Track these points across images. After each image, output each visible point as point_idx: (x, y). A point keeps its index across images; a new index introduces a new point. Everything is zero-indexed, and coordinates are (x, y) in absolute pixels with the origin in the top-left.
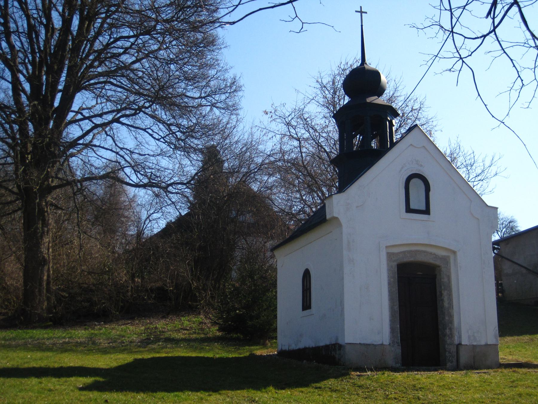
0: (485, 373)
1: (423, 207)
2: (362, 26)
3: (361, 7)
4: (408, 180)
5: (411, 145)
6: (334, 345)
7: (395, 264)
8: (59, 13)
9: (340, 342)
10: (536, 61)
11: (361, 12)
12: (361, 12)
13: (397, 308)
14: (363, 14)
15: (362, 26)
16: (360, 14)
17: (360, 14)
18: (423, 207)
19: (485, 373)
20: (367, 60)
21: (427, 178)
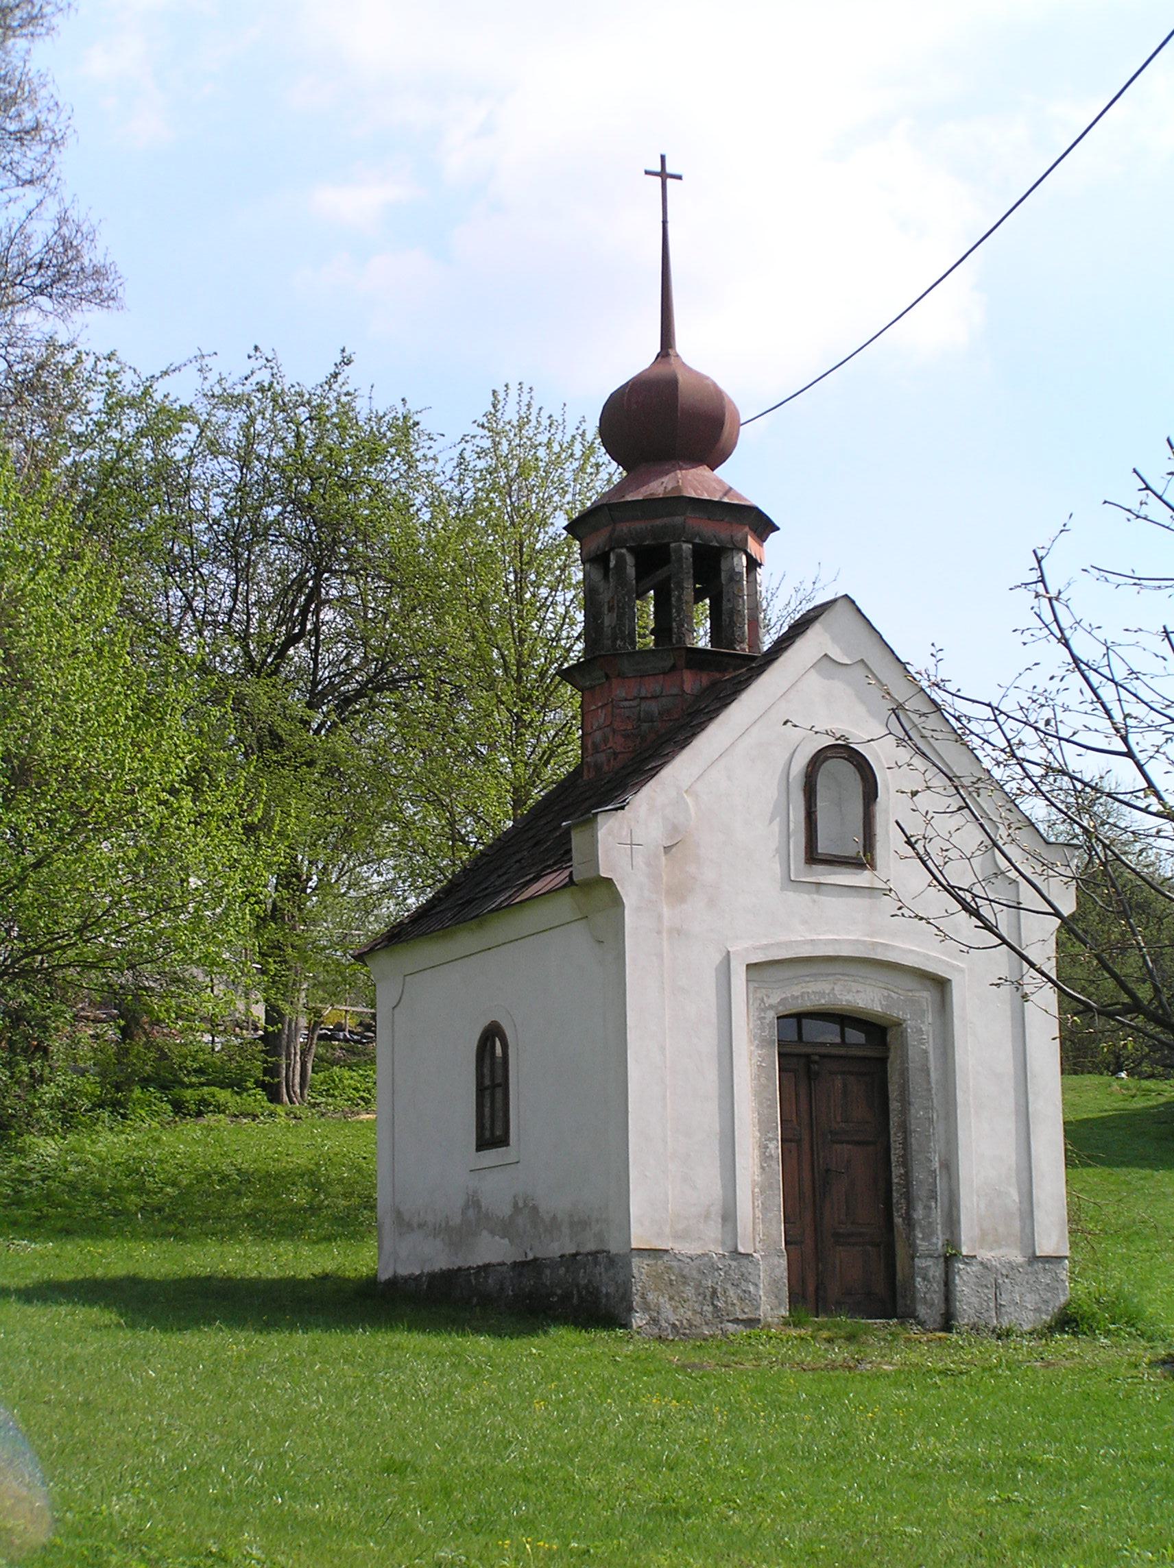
0: (1106, 1111)
1: (853, 847)
2: (665, 222)
3: (663, 158)
4: (818, 760)
5: (862, 661)
6: (594, 1254)
7: (771, 1015)
8: (1082, 662)
9: (614, 1248)
10: (1160, 498)
11: (663, 175)
12: (663, 175)
13: (776, 1148)
14: (658, 169)
15: (665, 222)
16: (659, 180)
17: (659, 180)
18: (853, 847)
19: (1106, 1111)
20: (683, 346)
21: (811, 756)
